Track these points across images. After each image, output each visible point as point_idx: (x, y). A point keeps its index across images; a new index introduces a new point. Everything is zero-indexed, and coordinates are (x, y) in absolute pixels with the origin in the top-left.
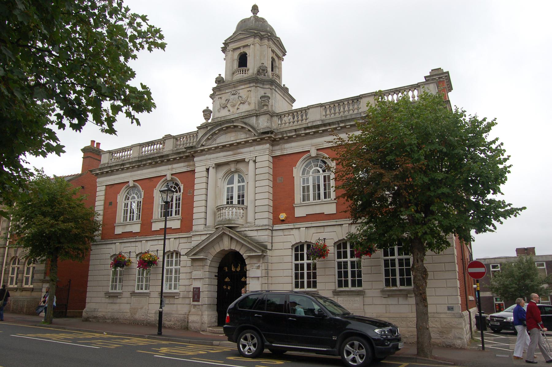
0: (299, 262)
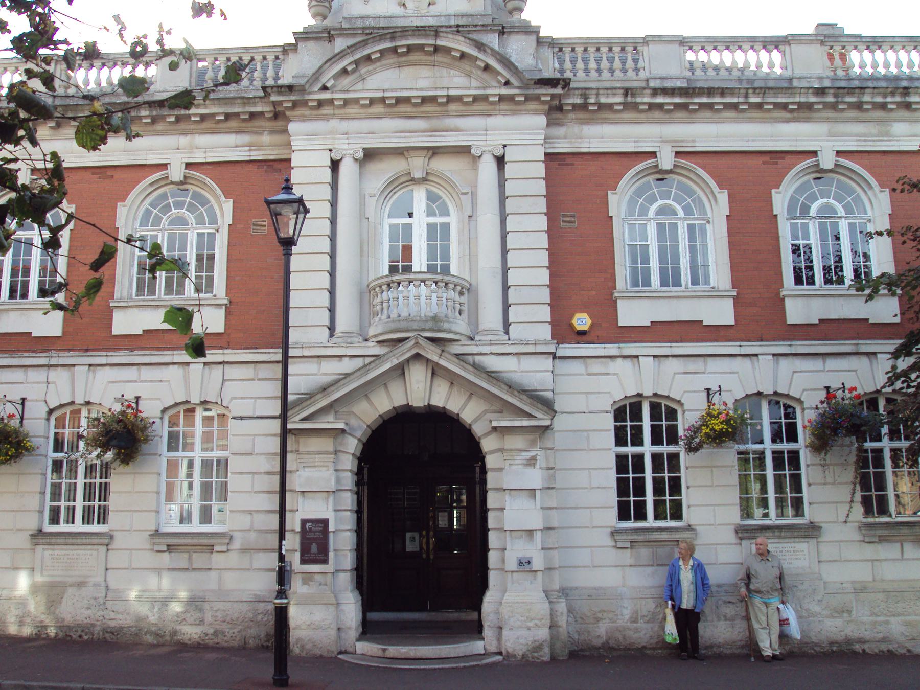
0: (630, 450)
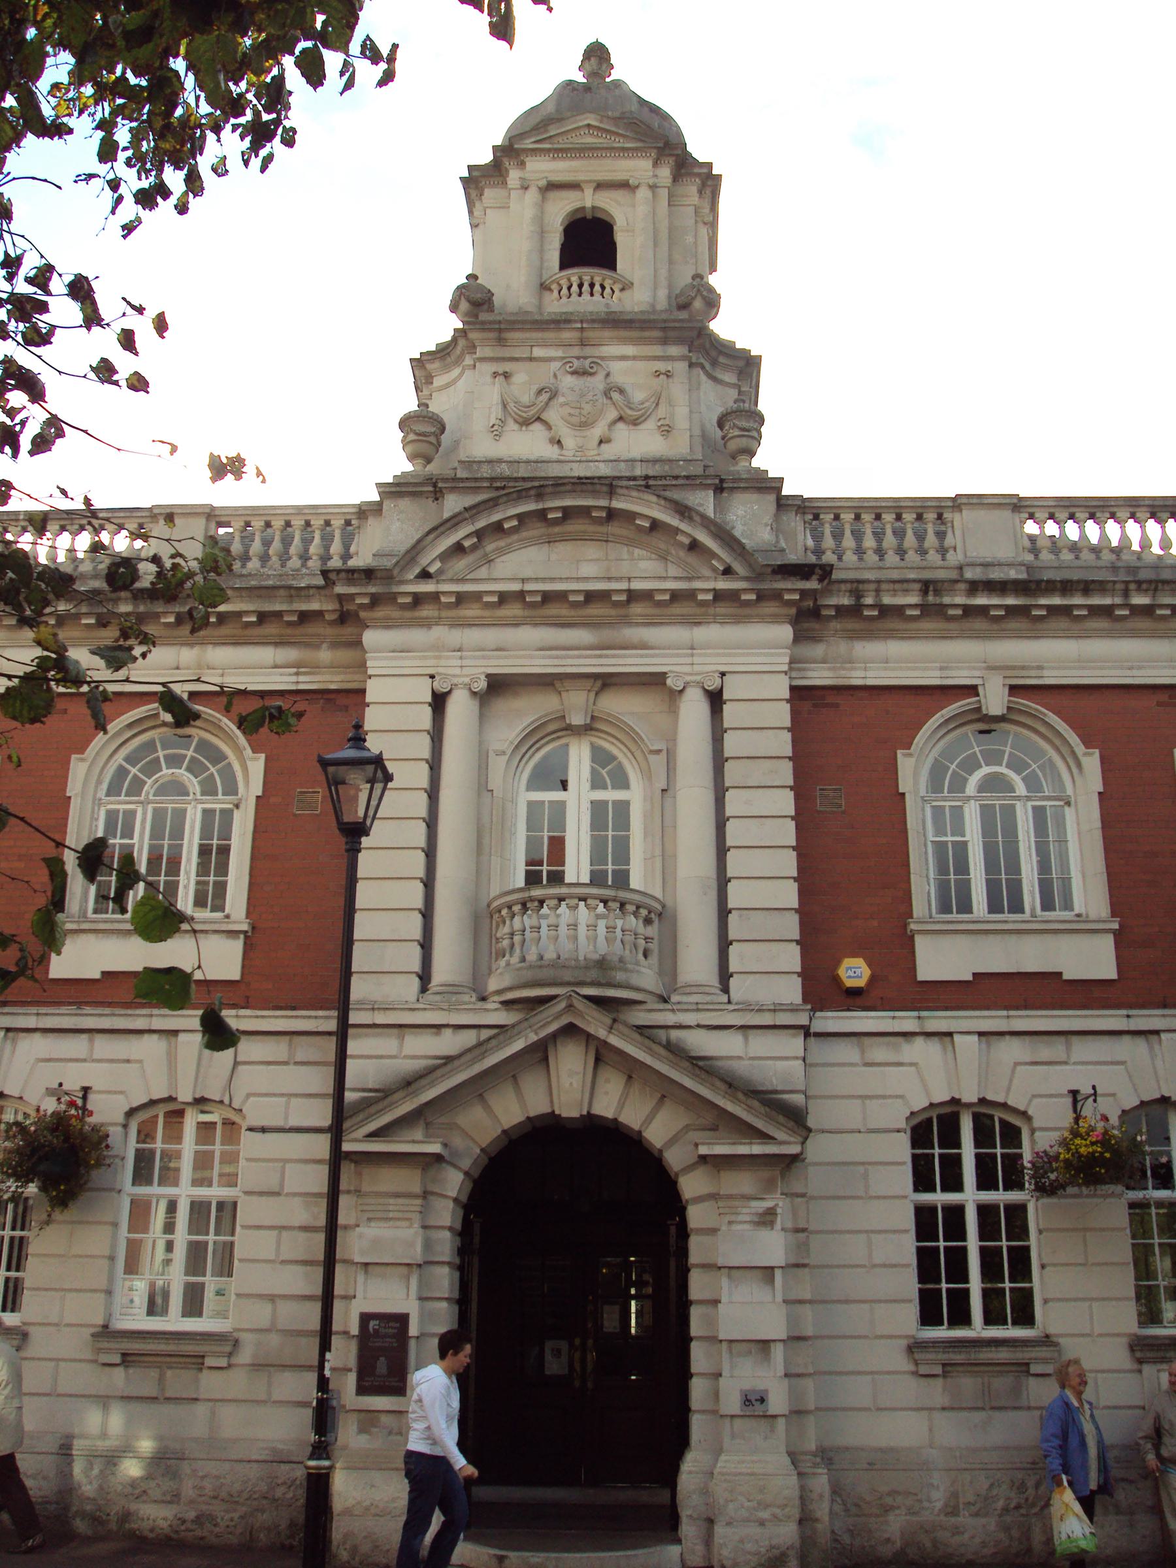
0: (939, 1198)
